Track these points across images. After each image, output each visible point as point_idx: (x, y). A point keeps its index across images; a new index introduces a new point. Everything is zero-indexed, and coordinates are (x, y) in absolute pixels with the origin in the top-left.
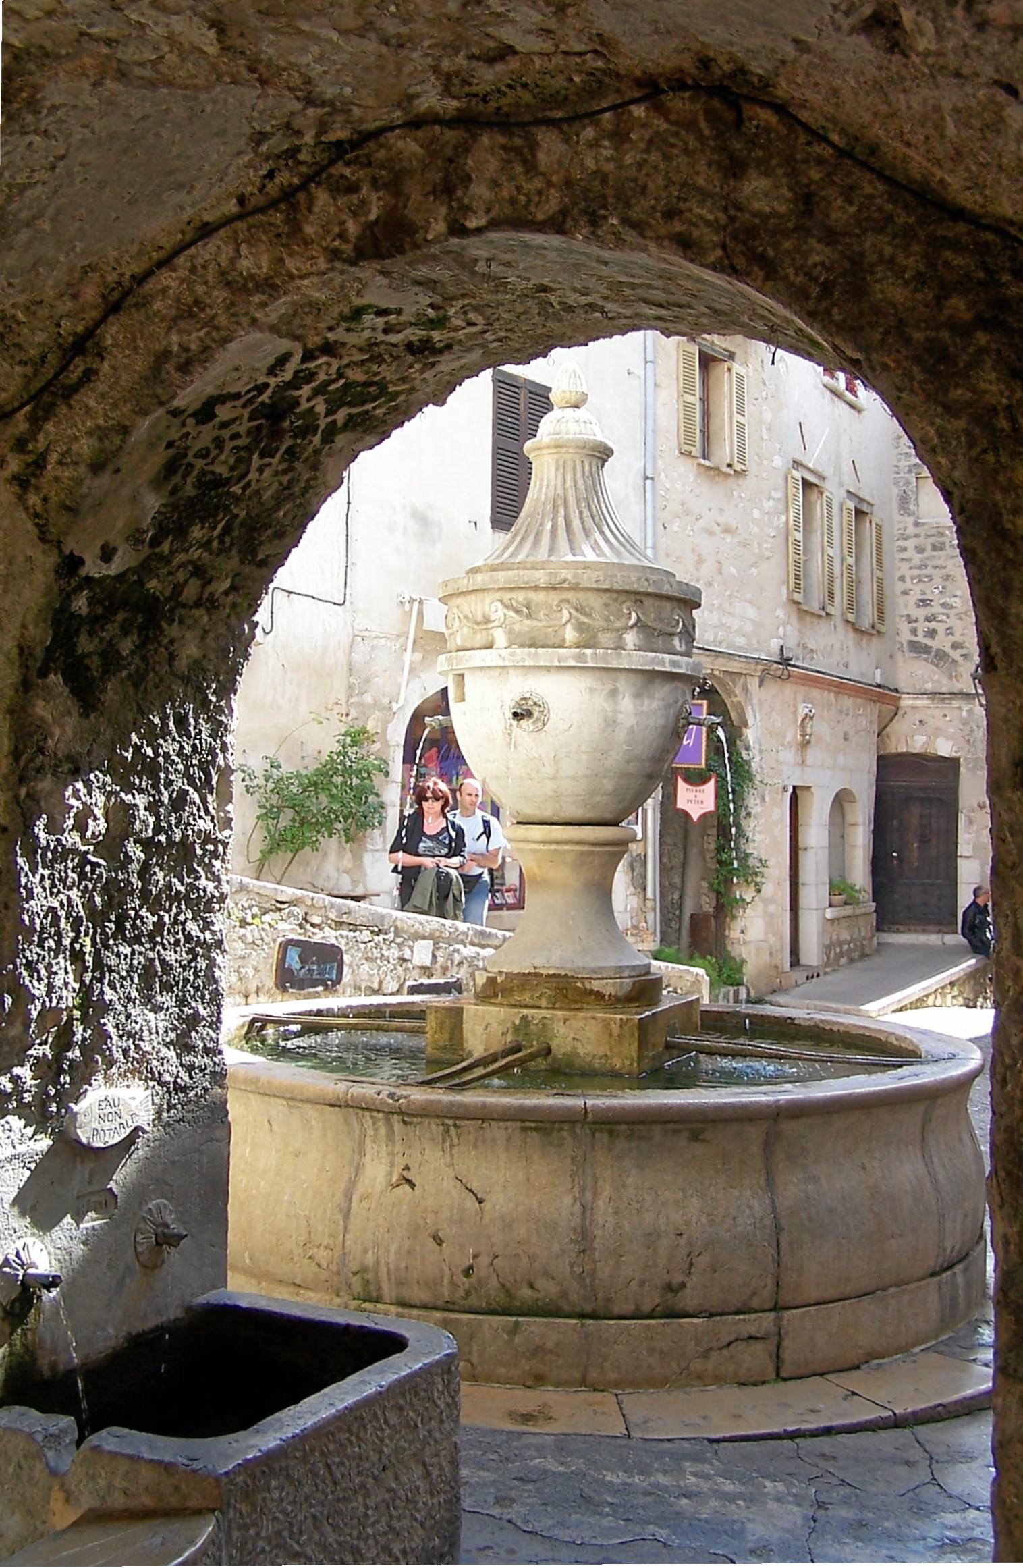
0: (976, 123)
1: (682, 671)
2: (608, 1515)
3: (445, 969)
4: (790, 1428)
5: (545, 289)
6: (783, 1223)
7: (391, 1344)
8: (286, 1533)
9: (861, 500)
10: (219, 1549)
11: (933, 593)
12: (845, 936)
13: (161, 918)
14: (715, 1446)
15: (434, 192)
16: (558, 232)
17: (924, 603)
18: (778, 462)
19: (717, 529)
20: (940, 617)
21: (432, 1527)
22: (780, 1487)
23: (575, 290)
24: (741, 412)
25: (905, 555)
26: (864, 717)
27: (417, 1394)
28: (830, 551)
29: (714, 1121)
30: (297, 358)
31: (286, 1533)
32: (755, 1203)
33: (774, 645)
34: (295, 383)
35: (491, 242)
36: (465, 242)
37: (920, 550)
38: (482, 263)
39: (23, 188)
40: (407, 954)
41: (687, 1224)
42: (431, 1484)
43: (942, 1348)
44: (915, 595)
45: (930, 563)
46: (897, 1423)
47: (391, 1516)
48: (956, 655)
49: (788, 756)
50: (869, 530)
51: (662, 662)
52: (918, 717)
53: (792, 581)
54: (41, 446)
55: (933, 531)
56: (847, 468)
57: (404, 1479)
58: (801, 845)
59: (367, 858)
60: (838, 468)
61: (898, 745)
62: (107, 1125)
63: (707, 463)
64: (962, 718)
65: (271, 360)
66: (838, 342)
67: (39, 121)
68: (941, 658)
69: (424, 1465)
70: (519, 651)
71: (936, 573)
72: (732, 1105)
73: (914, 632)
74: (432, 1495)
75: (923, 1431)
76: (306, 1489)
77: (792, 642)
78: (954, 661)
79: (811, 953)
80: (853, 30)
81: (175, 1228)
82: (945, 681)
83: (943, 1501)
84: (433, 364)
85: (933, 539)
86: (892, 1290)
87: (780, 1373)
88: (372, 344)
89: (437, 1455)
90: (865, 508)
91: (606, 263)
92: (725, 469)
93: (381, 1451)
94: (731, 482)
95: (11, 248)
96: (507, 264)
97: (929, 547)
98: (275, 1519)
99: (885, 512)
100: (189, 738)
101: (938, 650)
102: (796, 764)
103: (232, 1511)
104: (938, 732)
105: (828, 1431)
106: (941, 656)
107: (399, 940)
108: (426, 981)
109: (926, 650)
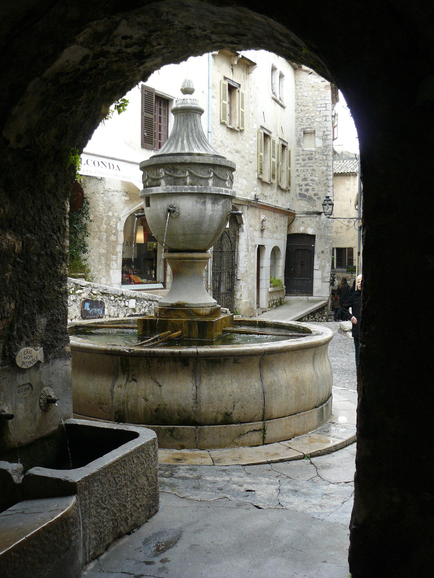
1: (229, 194)
2: (208, 491)
3: (140, 309)
4: (269, 460)
5: (189, 28)
6: (266, 391)
7: (135, 435)
8: (100, 501)
9: (284, 141)
10: (78, 507)
11: (308, 176)
12: (275, 298)
13: (44, 283)
14: (243, 467)
17: (305, 179)
19: (233, 152)
20: (310, 184)
21: (150, 497)
22: (267, 479)
23: (200, 28)
24: (243, 107)
25: (298, 162)
26: (283, 221)
27: (143, 452)
28: (273, 160)
29: (242, 356)
31: (100, 501)
32: (256, 384)
33: (253, 194)
37: (304, 160)
38: (165, 14)
40: (127, 304)
42: (149, 483)
44: (302, 176)
45: (307, 165)
46: (304, 457)
47: (136, 494)
48: (315, 198)
49: (257, 234)
50: (286, 153)
51: (222, 191)
52: (301, 220)
53: (259, 171)
55: (309, 153)
56: (279, 129)
57: (140, 481)
58: (261, 266)
59: (111, 272)
63: (230, 127)
64: (317, 221)
68: (310, 199)
69: (147, 476)
70: (170, 187)
71: (310, 169)
72: (249, 350)
73: (301, 190)
74: (149, 486)
75: (314, 460)
76: (107, 486)
77: (258, 193)
78: (315, 200)
79: (264, 303)
82: (311, 207)
83: (321, 481)
85: (308, 156)
86: (302, 413)
88: (119, 52)
89: (151, 473)
90: (285, 144)
91: (214, 13)
92: (237, 129)
93: (132, 472)
94: (239, 134)
96: (175, 15)
97: (307, 159)
98: (96, 496)
99: (291, 146)
100: (52, 214)
101: (309, 196)
102: (260, 237)
103: (81, 494)
104: (308, 226)
105: (282, 461)
106: (310, 198)
107: (124, 299)
108: (134, 314)
109: (305, 196)
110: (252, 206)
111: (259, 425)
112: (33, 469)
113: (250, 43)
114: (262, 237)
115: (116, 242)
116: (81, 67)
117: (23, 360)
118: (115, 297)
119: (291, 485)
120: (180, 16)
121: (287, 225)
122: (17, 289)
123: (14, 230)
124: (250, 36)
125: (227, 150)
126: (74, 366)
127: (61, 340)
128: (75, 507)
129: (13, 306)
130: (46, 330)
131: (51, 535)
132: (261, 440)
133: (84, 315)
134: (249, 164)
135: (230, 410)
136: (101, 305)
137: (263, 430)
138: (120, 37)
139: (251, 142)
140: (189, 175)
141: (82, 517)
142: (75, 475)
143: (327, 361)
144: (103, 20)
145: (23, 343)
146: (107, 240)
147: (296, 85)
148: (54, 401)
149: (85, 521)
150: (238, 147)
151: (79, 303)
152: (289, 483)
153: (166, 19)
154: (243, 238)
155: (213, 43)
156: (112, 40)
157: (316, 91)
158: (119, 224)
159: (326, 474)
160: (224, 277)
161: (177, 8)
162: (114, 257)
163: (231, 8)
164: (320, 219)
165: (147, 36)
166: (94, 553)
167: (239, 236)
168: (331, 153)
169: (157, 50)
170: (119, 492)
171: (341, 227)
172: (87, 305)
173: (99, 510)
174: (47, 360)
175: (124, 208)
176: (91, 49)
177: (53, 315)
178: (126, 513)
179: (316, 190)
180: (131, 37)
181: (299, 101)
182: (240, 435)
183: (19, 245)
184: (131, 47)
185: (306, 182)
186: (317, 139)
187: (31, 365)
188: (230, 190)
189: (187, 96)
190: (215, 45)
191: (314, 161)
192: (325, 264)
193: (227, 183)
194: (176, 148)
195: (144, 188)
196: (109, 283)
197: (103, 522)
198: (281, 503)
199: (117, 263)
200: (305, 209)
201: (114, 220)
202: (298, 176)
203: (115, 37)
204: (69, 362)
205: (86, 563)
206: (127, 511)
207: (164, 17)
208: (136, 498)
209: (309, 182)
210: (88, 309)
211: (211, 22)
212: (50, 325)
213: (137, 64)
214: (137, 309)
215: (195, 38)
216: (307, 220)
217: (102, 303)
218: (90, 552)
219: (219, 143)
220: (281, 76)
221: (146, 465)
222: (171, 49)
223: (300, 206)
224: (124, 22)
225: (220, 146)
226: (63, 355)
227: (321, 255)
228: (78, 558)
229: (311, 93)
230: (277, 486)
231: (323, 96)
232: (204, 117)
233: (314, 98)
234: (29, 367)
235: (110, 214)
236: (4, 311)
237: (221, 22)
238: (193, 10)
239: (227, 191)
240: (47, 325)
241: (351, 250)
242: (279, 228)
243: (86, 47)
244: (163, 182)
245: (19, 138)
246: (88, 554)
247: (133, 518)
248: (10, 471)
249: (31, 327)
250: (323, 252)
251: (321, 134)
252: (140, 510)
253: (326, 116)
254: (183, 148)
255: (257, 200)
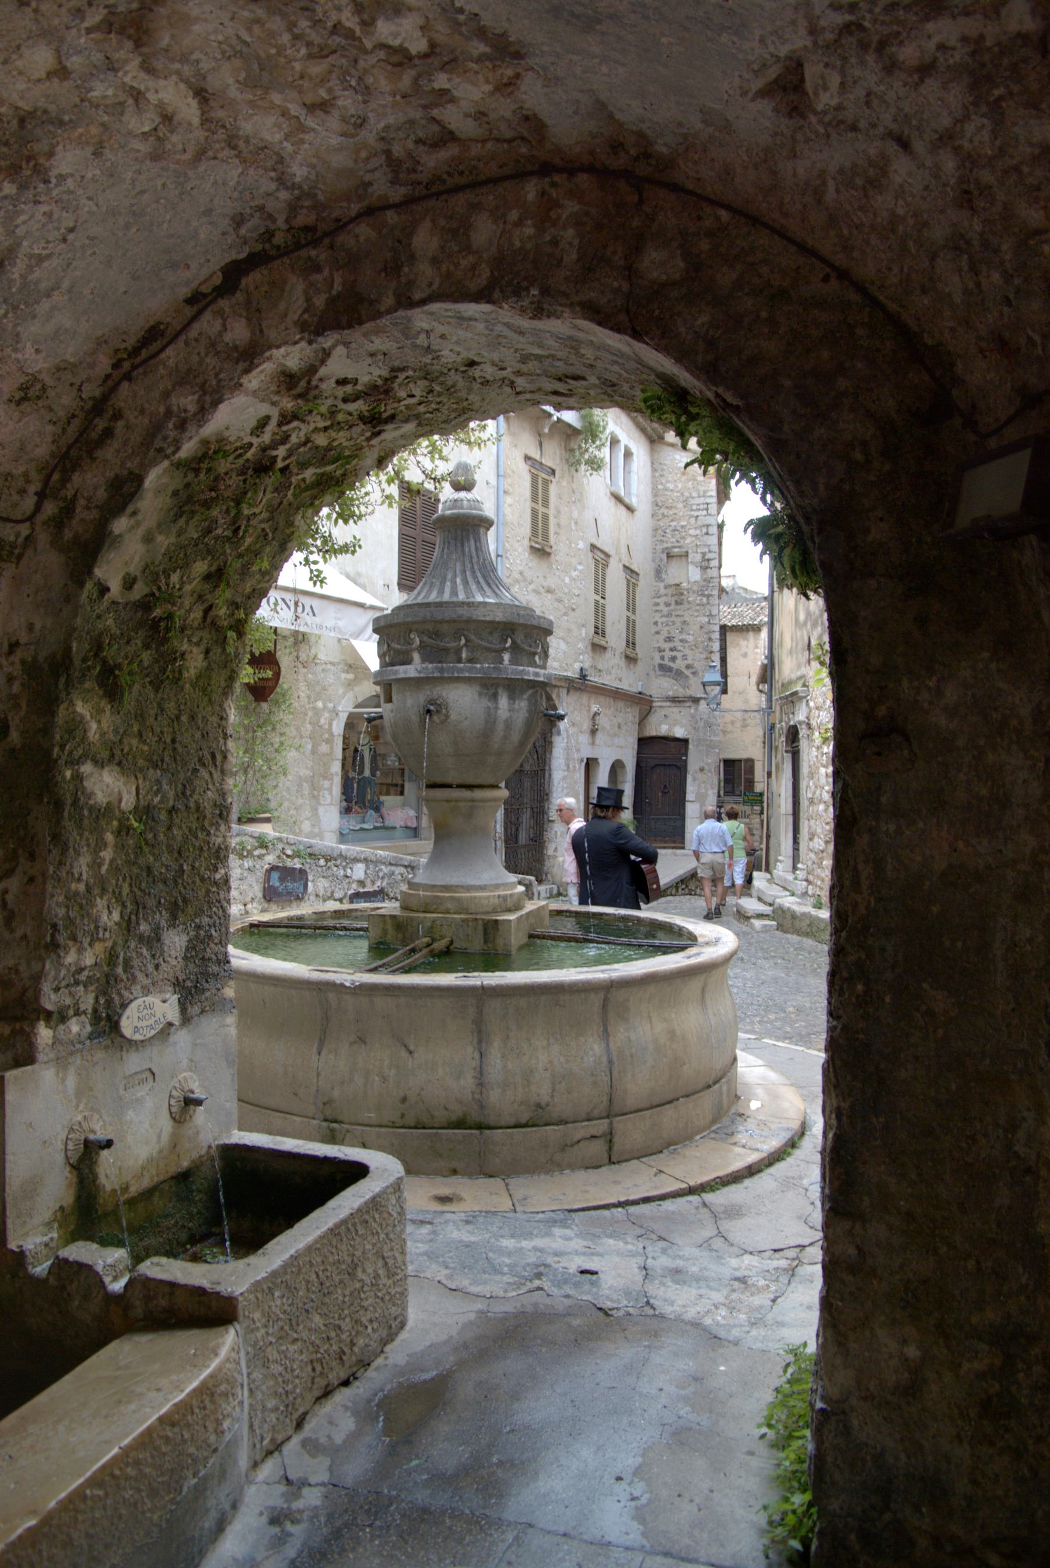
0: (859, 181)
5: (472, 364)
7: (357, 1172)
8: (287, 1328)
15: (385, 269)
16: (488, 302)
17: (669, 639)
18: (581, 545)
19: (542, 591)
23: (494, 364)
26: (630, 715)
30: (274, 422)
31: (287, 1328)
32: (596, 1047)
33: (577, 666)
34: (274, 445)
35: (432, 314)
36: (409, 313)
37: (667, 605)
38: (423, 336)
39: (41, 259)
41: (551, 1062)
43: (713, 1135)
44: (664, 633)
46: (691, 1191)
48: (688, 672)
49: (585, 739)
51: (528, 673)
54: (69, 494)
56: (624, 550)
59: (321, 810)
60: (618, 553)
61: (652, 731)
62: (145, 1023)
65: (253, 423)
66: (720, 391)
67: (49, 190)
71: (678, 620)
73: (662, 658)
75: (708, 1197)
77: (587, 665)
80: (762, 94)
81: (198, 1094)
84: (379, 433)
87: (613, 1157)
89: (392, 1250)
95: (34, 317)
105: (646, 1200)
109: (670, 669)
110: (576, 689)
111: (600, 1126)
112: (148, 1262)
113: (592, 393)
114: (593, 743)
115: (330, 754)
116: (255, 441)
117: (136, 1023)
118: (327, 861)
119: (668, 1256)
120: (454, 339)
121: (637, 720)
122: (124, 880)
123: (119, 764)
124: (593, 380)
125: (531, 587)
126: (241, 1025)
127: (216, 976)
128: (234, 1355)
129: (116, 916)
130: (185, 958)
131: (177, 1429)
132: (606, 1155)
133: (270, 895)
134: (571, 613)
135: (545, 1099)
136: (301, 875)
137: (609, 1137)
138: (333, 380)
139: (574, 574)
140: (465, 645)
141: (248, 1367)
142: (233, 1275)
143: (727, 994)
144: (298, 346)
145: (137, 989)
146: (314, 751)
147: (654, 470)
148: (199, 1102)
149: (254, 1375)
150: (551, 582)
151: (260, 874)
152: (664, 1251)
153: (426, 345)
154: (560, 746)
155: (518, 393)
156: (317, 387)
157: (689, 480)
158: (335, 723)
159: (736, 1230)
160: (526, 818)
161: (449, 323)
162: (326, 784)
163: (559, 322)
164: (696, 709)
165: (386, 380)
166: (273, 1440)
167: (551, 743)
168: (716, 592)
169: (408, 407)
170: (327, 1300)
171: (733, 723)
172: (275, 875)
173: (284, 1348)
174: (186, 1019)
175: (345, 693)
176: (274, 404)
177: (199, 927)
178: (340, 1341)
179: (690, 658)
180: (356, 382)
181: (659, 499)
182: (564, 1148)
183: (129, 792)
184: (354, 401)
185: (671, 645)
186: (691, 568)
187: (153, 1032)
188: (542, 672)
189: (463, 495)
190: (521, 397)
191: (686, 606)
192: (706, 789)
193: (537, 658)
194: (441, 592)
195: (381, 667)
196: (316, 830)
197: (292, 1370)
198: (652, 1301)
199: (331, 794)
200: (671, 693)
201: (326, 715)
202: (657, 633)
203: (321, 380)
204: (231, 1020)
205: (255, 1465)
206: (344, 1337)
207: (422, 340)
208: (362, 1307)
209: (677, 644)
210: (277, 884)
211: (516, 350)
212: (194, 948)
213: (368, 434)
214: (368, 882)
215: (482, 384)
216: (674, 711)
217: (302, 872)
218: (263, 1438)
219: (517, 576)
220: (628, 454)
221: (382, 1236)
222: (434, 406)
223: (661, 687)
224: (340, 350)
225: (517, 581)
226: (219, 1006)
227: (699, 775)
228: (236, 1462)
229: (680, 485)
230: (640, 1260)
231: (702, 489)
232: (491, 534)
233: (686, 494)
234: (149, 1035)
235: (320, 704)
236: (97, 927)
237: (537, 351)
238: (480, 327)
239: (537, 674)
240: (187, 949)
241: (750, 762)
242: (624, 728)
243: (263, 401)
244: (416, 656)
245: (129, 583)
246: (258, 1446)
247: (356, 1349)
248: (99, 1268)
249: (153, 956)
250: (702, 770)
251: (698, 558)
252: (370, 1330)
253: (708, 526)
254: (454, 592)
255: (583, 677)
